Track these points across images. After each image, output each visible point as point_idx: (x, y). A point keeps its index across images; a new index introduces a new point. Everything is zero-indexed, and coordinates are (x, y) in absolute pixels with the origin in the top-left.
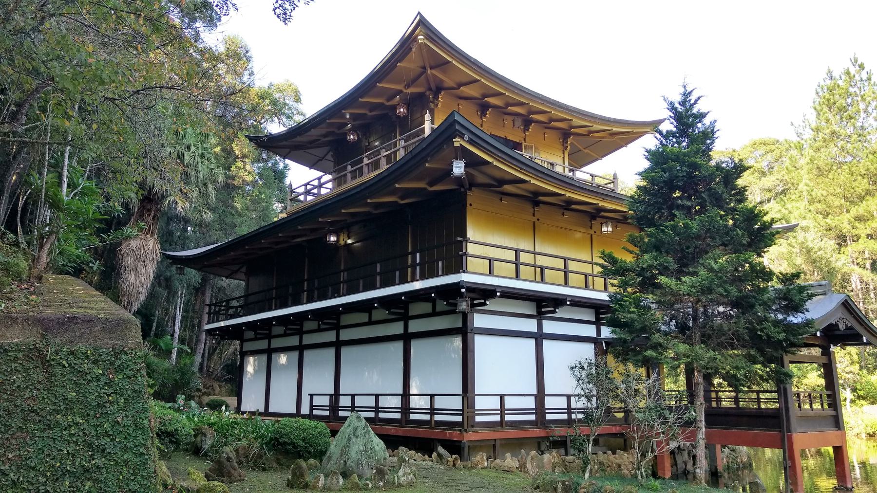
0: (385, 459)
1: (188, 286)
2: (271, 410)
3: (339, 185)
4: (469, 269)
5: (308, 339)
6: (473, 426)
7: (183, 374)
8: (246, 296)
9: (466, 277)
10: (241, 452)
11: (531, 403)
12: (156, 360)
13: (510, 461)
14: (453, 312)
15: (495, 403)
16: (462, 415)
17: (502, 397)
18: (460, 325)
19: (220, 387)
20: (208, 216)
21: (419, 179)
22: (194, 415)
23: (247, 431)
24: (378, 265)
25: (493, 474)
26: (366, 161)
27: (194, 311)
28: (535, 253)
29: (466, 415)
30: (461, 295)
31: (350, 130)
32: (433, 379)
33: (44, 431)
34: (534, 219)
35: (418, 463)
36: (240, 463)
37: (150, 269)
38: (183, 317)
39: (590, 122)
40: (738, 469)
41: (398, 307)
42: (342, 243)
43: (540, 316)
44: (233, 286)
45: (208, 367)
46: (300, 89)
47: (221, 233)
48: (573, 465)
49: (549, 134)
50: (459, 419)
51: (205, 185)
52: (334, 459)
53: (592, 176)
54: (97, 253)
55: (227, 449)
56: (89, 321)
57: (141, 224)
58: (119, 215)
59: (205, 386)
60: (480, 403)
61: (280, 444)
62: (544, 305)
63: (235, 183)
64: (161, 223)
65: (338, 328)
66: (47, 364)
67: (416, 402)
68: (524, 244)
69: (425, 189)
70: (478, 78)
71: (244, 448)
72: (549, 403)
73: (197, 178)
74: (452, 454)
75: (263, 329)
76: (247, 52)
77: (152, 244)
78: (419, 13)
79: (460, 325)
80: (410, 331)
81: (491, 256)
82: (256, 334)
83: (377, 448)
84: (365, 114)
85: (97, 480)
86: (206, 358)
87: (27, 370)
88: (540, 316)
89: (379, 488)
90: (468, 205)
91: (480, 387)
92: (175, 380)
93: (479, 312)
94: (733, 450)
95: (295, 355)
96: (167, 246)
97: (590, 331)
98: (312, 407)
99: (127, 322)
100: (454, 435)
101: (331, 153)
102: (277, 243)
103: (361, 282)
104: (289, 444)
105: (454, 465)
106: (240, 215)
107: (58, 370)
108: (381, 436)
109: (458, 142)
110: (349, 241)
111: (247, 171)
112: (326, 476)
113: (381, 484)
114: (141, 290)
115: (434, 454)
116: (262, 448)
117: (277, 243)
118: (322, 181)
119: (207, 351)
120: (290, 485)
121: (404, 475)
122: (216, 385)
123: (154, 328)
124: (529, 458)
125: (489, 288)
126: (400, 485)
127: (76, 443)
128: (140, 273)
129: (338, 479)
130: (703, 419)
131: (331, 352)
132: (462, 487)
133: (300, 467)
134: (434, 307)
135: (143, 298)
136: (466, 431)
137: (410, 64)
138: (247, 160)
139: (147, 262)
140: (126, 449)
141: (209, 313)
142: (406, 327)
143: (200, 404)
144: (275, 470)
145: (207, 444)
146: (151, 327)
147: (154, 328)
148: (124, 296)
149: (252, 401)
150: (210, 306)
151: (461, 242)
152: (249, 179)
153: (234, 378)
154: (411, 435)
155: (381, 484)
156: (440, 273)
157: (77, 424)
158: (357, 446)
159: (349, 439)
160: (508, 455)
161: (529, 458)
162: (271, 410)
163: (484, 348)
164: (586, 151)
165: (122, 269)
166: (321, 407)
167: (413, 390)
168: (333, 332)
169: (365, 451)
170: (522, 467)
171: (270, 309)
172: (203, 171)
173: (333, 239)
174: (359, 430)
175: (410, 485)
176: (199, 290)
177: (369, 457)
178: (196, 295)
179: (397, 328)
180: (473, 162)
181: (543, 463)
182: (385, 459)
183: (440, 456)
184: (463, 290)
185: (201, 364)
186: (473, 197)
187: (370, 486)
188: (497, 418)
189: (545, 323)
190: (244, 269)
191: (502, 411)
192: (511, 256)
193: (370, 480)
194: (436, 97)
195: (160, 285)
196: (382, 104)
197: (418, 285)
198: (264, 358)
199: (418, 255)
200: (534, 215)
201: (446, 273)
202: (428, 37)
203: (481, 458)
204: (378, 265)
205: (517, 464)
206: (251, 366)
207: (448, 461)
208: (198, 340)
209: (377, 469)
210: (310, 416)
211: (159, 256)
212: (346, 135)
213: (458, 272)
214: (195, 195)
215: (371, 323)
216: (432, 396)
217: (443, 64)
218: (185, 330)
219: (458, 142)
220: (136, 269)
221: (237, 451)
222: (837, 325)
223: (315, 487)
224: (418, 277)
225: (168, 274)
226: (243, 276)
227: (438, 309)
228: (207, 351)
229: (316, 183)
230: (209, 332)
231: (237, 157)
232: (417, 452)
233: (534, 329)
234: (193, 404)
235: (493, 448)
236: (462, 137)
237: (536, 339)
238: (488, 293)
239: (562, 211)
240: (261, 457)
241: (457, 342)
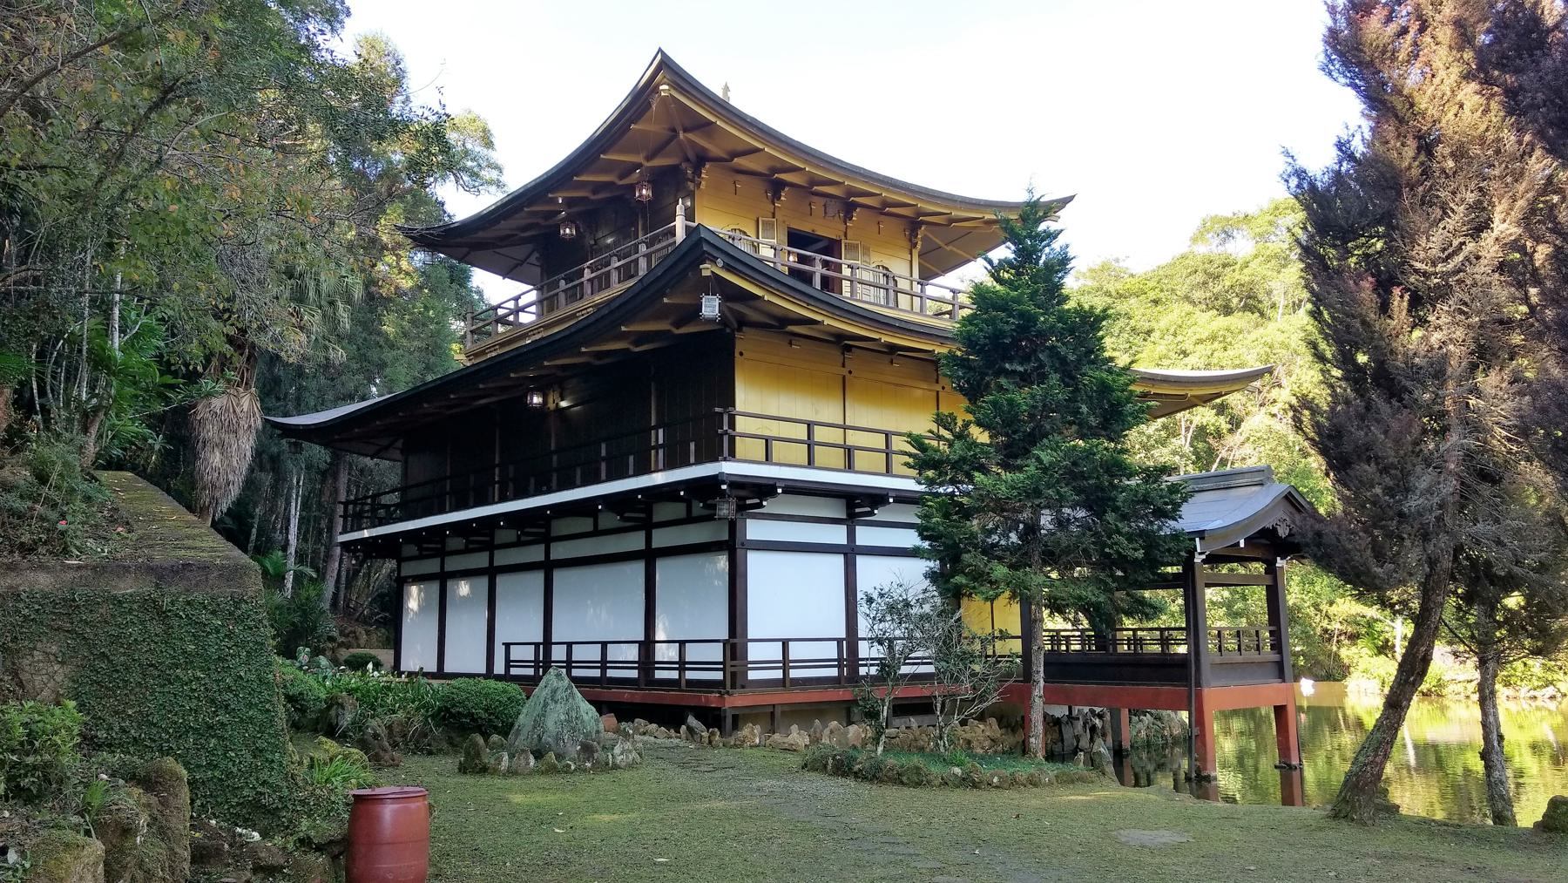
1: (308, 468)
2: (448, 669)
3: (551, 310)
4: (738, 454)
5: (502, 558)
7: (305, 614)
8: (403, 490)
9: (728, 468)
10: (396, 729)
14: (709, 518)
15: (775, 652)
16: (723, 670)
17: (785, 643)
18: (726, 537)
19: (368, 633)
20: (339, 354)
21: (658, 317)
22: (325, 678)
23: (405, 699)
24: (603, 446)
26: (587, 274)
27: (320, 504)
28: (845, 428)
29: (729, 670)
30: (722, 494)
31: (564, 220)
32: (688, 621)
33: (163, 686)
34: (844, 371)
36: (395, 745)
37: (245, 445)
38: (301, 519)
40: (1164, 747)
41: (636, 511)
42: (552, 406)
43: (851, 520)
44: (386, 472)
45: (347, 601)
46: (490, 126)
47: (361, 377)
49: (887, 225)
50: (719, 676)
51: (332, 303)
52: (524, 732)
53: (953, 291)
54: (155, 422)
55: (373, 723)
56: (205, 568)
57: (230, 374)
59: (342, 633)
60: (755, 652)
61: (453, 716)
62: (858, 505)
63: (384, 292)
64: (261, 366)
65: (547, 540)
66: (163, 615)
67: (666, 653)
68: (828, 410)
70: (760, 146)
71: (400, 724)
73: (318, 292)
75: (431, 542)
76: (398, 63)
77: (247, 402)
78: (660, 50)
79: (726, 537)
81: (767, 433)
82: (420, 549)
83: (586, 718)
85: (222, 738)
86: (343, 586)
87: (142, 622)
88: (851, 520)
89: (585, 770)
92: (293, 624)
94: (1158, 718)
96: (272, 402)
98: (508, 663)
99: (245, 567)
101: (536, 255)
102: (449, 407)
103: (579, 472)
104: (465, 716)
106: (392, 346)
107: (175, 622)
108: (590, 702)
109: (707, 269)
110: (564, 404)
111: (405, 268)
112: (511, 756)
113: (588, 765)
114: (231, 478)
115: (684, 727)
116: (426, 723)
117: (449, 407)
118: (522, 303)
119: (344, 573)
120: (463, 770)
122: (360, 630)
123: (253, 537)
126: (616, 767)
127: (198, 698)
128: (227, 459)
130: (1042, 669)
131: (538, 578)
133: (476, 745)
135: (235, 491)
139: (241, 432)
140: (250, 706)
141: (345, 517)
143: (335, 662)
144: (447, 754)
145: (347, 719)
146: (249, 534)
147: (253, 537)
148: (204, 488)
149: (417, 653)
150: (346, 504)
151: (721, 414)
152: (407, 284)
154: (649, 699)
156: (692, 460)
157: (198, 679)
158: (556, 715)
159: (546, 705)
160: (795, 727)
162: (448, 669)
164: (949, 248)
166: (522, 663)
167: (660, 635)
168: (542, 548)
171: (442, 511)
172: (328, 281)
173: (537, 400)
175: (631, 766)
176: (328, 474)
178: (323, 482)
179: (636, 542)
180: (731, 295)
183: (690, 730)
184: (724, 487)
185: (335, 596)
186: (745, 343)
188: (778, 674)
190: (399, 444)
191: (786, 663)
192: (800, 432)
193: (572, 760)
194: (697, 173)
195: (262, 469)
196: (612, 183)
197: (659, 478)
201: (700, 461)
202: (675, 86)
203: (752, 732)
204: (603, 446)
206: (414, 598)
208: (328, 557)
209: (582, 744)
210: (506, 677)
211: (259, 422)
212: (558, 228)
214: (314, 320)
215: (596, 533)
216: (682, 643)
217: (704, 126)
218: (305, 540)
219: (707, 269)
220: (222, 445)
221: (389, 728)
222: (1274, 530)
225: (275, 450)
226: (397, 454)
228: (344, 573)
229: (511, 305)
230: (346, 546)
231: (384, 247)
234: (323, 661)
235: (771, 718)
237: (845, 555)
238: (765, 489)
239: (888, 358)
240: (425, 736)
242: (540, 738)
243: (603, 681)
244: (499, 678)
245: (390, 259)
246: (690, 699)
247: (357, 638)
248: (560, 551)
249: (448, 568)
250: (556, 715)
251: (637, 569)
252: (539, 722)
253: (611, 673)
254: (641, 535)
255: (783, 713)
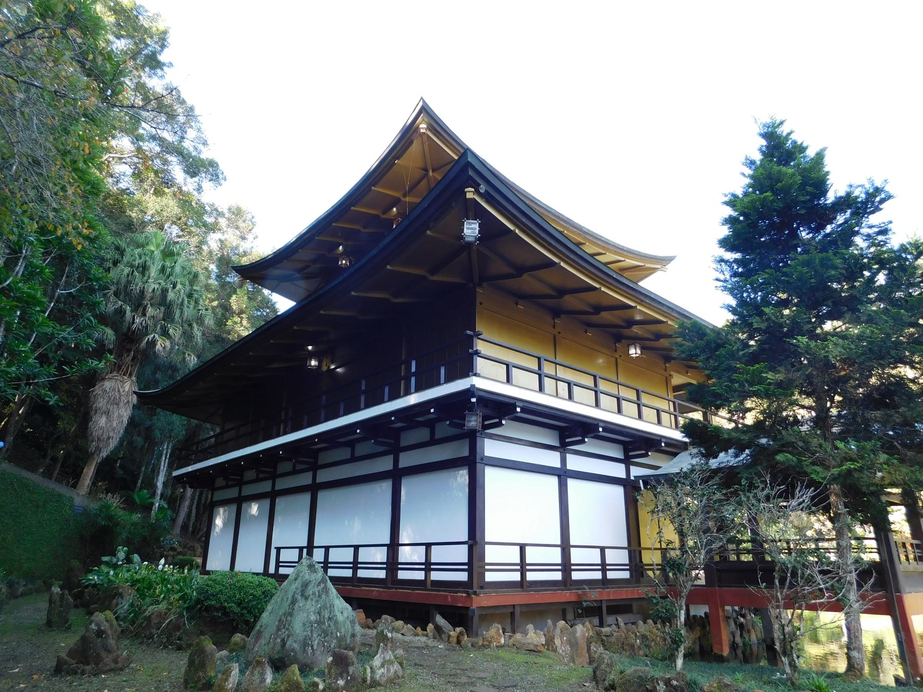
0: (353, 635)
5: (281, 484)
6: (482, 588)
11: (555, 556)
12: (121, 513)
13: (533, 636)
17: (522, 547)
18: (466, 453)
24: (364, 382)
25: (520, 658)
34: (555, 332)
35: (407, 638)
37: (124, 414)
42: (324, 368)
43: (563, 447)
51: (190, 325)
58: (87, 349)
60: (491, 555)
67: (406, 554)
69: (424, 277)
72: (577, 556)
74: (455, 625)
79: (466, 453)
83: (340, 618)
90: (478, 304)
91: (491, 532)
95: (267, 503)
97: (618, 470)
98: (278, 564)
104: (217, 610)
105: (459, 642)
108: (348, 600)
113: (341, 682)
114: (111, 434)
115: (430, 626)
116: (181, 615)
124: (558, 631)
126: (375, 684)
129: (262, 674)
134: (432, 433)
135: (113, 444)
136: (475, 593)
138: (244, 316)
139: (121, 404)
142: (396, 462)
148: (92, 441)
149: (217, 561)
153: (200, 535)
154: (392, 599)
158: (306, 612)
159: (294, 602)
160: (530, 627)
161: (558, 631)
165: (93, 412)
167: (404, 538)
169: (320, 622)
170: (549, 643)
175: (393, 681)
177: (325, 633)
180: (490, 229)
181: (576, 638)
182: (353, 635)
183: (438, 629)
184: (474, 400)
188: (516, 577)
189: (570, 458)
191: (523, 566)
198: (234, 508)
199: (414, 363)
200: (554, 327)
201: (450, 379)
204: (364, 382)
205: (543, 640)
207: (449, 636)
213: (468, 376)
215: (353, 459)
216: (428, 546)
220: (107, 413)
232: (406, 623)
233: (558, 465)
236: (476, 186)
237: (559, 476)
241: (462, 476)
243: (354, 580)
244: (271, 576)
245: (237, 319)
248: (324, 476)
249: (244, 493)
250: (306, 612)
252: (284, 623)
253: (362, 574)
255: (522, 613)
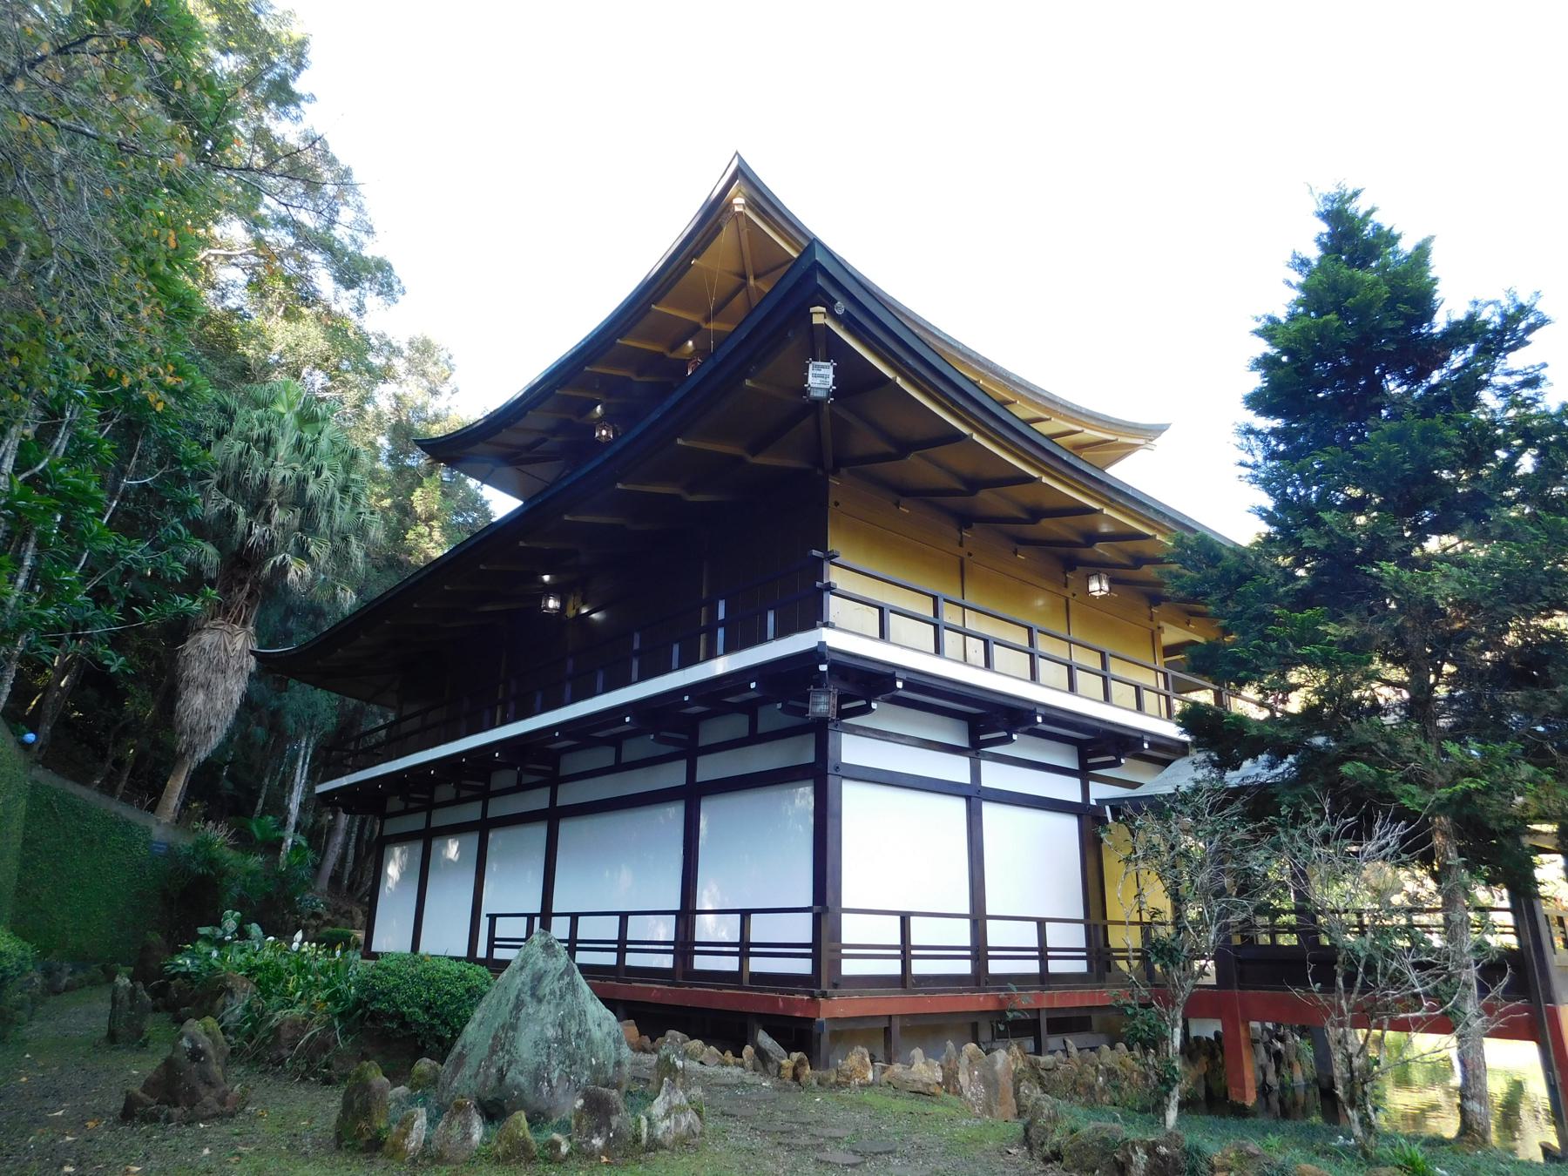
0: (618, 1064)
5: (498, 808)
6: (835, 986)
13: (922, 1068)
17: (905, 918)
18: (810, 758)
24: (637, 637)
31: (601, 419)
34: (963, 552)
35: (709, 1070)
37: (234, 688)
39: (1046, 410)
42: (571, 613)
43: (974, 749)
48: (1057, 1076)
51: (345, 539)
52: (472, 1061)
60: (852, 930)
67: (708, 928)
72: (997, 934)
74: (789, 1049)
79: (810, 758)
80: (699, 779)
83: (597, 1034)
84: (628, 379)
88: (974, 749)
89: (590, 1155)
90: (831, 504)
91: (854, 888)
93: (853, 730)
95: (473, 839)
100: (781, 1002)
104: (391, 1018)
105: (796, 1077)
108: (609, 1003)
113: (598, 1142)
114: (213, 722)
115: (748, 1050)
116: (330, 1027)
121: (667, 1115)
124: (964, 1060)
125: (881, 669)
126: (655, 1145)
129: (466, 1126)
132: (838, 1156)
134: (753, 725)
135: (216, 739)
136: (824, 995)
137: (719, 260)
138: (434, 523)
139: (230, 672)
148: (181, 734)
154: (682, 1004)
155: (598, 1142)
158: (539, 1024)
159: (519, 1005)
160: (917, 1053)
161: (964, 1060)
163: (857, 804)
165: (182, 686)
167: (704, 901)
169: (562, 1041)
170: (950, 1080)
174: (546, 981)
175: (686, 1142)
177: (571, 1059)
181: (994, 1073)
182: (618, 1064)
183: (762, 1054)
184: (823, 668)
187: (564, 1149)
189: (986, 766)
191: (906, 951)
193: (564, 1127)
198: (418, 847)
200: (961, 544)
201: (783, 631)
204: (637, 637)
207: (780, 1067)
213: (814, 627)
215: (619, 767)
216: (745, 914)
220: (207, 686)
223: (398, 1149)
224: (720, 649)
227: (762, 728)
232: (707, 1044)
235: (886, 1036)
236: (829, 304)
237: (968, 798)
241: (803, 797)
242: (501, 1075)
243: (620, 971)
244: (481, 962)
246: (760, 1001)
247: (352, 919)
248: (570, 795)
251: (674, 814)
252: (501, 1042)
253: (632, 960)
254: (681, 766)
